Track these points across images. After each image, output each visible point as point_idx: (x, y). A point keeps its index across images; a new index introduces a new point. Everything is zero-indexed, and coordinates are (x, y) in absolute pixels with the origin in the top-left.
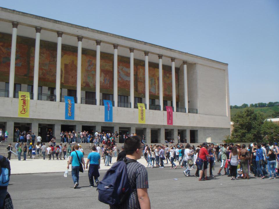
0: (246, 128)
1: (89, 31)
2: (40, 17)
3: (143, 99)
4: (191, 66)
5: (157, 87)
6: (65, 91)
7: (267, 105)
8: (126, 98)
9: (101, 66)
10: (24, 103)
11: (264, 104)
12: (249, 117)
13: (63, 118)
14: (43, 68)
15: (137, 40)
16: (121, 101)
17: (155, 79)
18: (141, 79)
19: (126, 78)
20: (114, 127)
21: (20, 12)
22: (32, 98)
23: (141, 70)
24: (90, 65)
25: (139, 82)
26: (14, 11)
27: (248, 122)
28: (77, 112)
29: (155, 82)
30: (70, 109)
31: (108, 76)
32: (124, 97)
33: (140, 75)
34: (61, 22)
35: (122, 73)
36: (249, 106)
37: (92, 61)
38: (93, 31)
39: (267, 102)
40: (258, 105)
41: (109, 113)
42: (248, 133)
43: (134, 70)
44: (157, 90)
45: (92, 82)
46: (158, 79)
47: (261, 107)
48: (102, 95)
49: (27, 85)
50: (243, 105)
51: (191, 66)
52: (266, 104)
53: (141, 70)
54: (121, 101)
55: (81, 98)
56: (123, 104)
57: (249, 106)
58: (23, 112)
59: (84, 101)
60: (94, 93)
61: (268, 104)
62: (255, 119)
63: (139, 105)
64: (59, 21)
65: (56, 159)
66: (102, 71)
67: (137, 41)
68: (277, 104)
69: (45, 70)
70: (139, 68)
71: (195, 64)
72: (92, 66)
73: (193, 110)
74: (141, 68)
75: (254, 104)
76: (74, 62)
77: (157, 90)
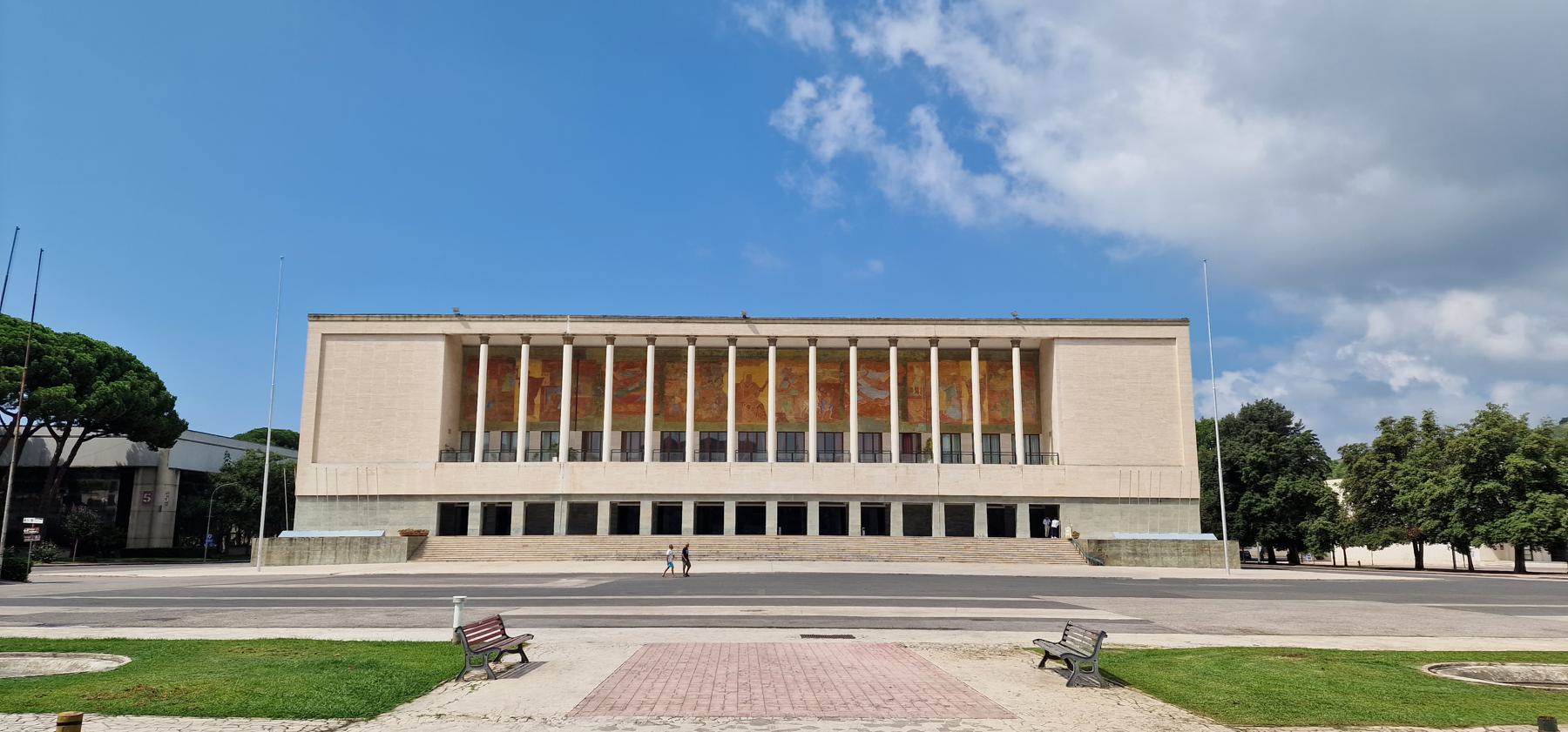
5: (965, 404)
9: (818, 377)
17: (960, 386)
18: (917, 392)
19: (879, 395)
20: (653, 533)
23: (916, 371)
24: (786, 379)
25: (913, 397)
29: (960, 393)
31: (828, 394)
33: (916, 383)
35: (864, 384)
37: (791, 369)
43: (899, 374)
44: (965, 411)
45: (791, 413)
46: (969, 386)
53: (918, 372)
55: (983, 452)
56: (870, 456)
59: (658, 455)
65: (741, 646)
66: (819, 386)
70: (912, 368)
72: (791, 381)
73: (1037, 455)
74: (917, 367)
76: (751, 378)
77: (965, 411)
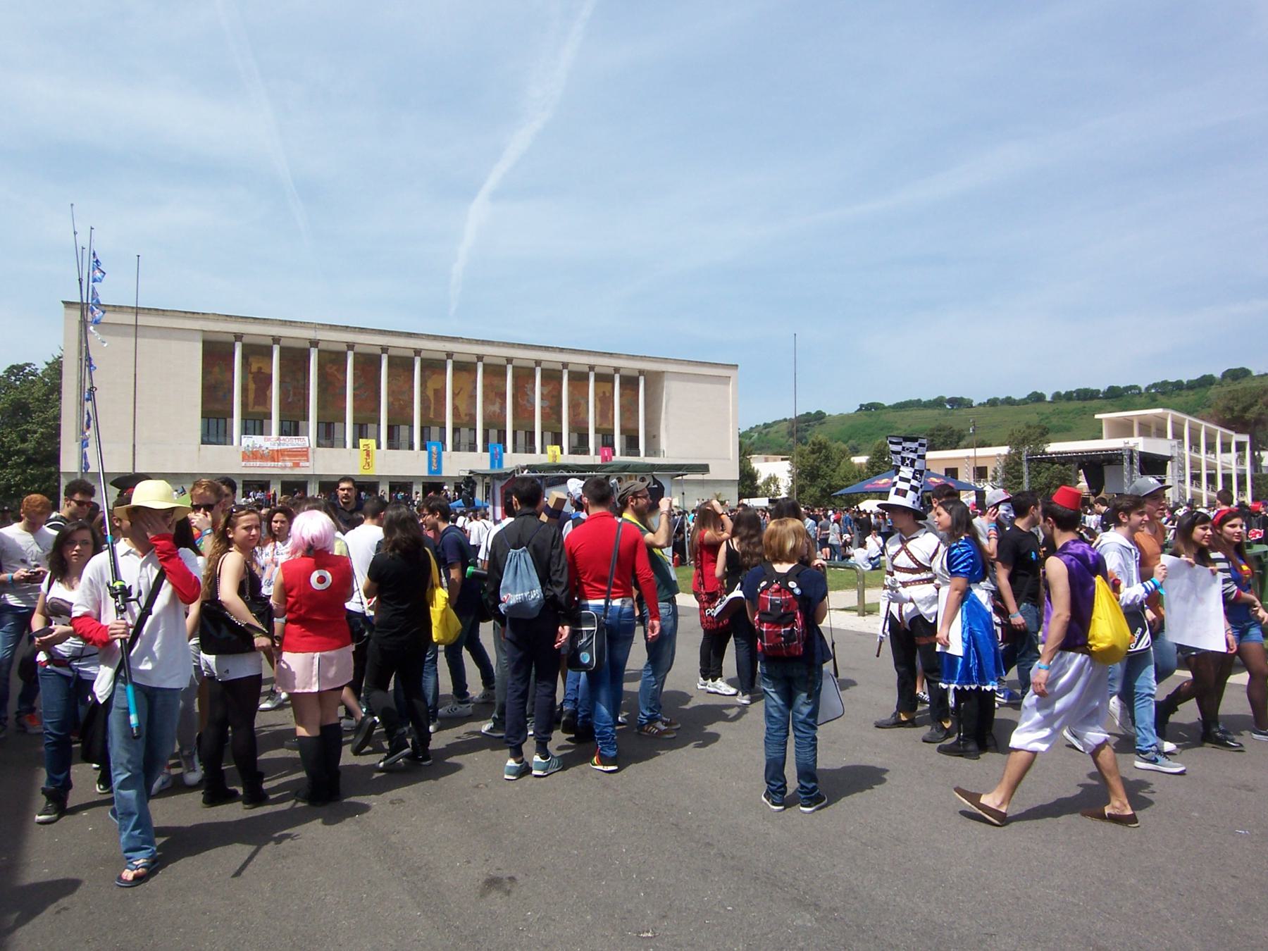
0: (807, 476)
1: (463, 342)
2: (385, 331)
3: (302, 423)
4: (654, 379)
6: (548, 435)
7: (1101, 395)
8: (222, 422)
10: (368, 455)
11: (1093, 391)
12: (815, 456)
13: (426, 474)
14: (400, 397)
15: (545, 347)
16: (208, 432)
21: (356, 328)
22: (378, 447)
26: (347, 327)
27: (811, 466)
28: (445, 463)
30: (435, 461)
32: (215, 420)
34: (417, 334)
36: (1048, 398)
38: (470, 341)
39: (1002, 396)
40: (1075, 395)
41: (497, 459)
42: (811, 485)
47: (1085, 399)
48: (625, 441)
49: (438, 428)
50: (1030, 397)
51: (654, 379)
52: (1099, 391)
54: (208, 432)
57: (1048, 398)
58: (367, 467)
60: (637, 438)
61: (1104, 393)
62: (827, 458)
63: (362, 442)
64: (414, 334)
67: (547, 348)
68: (1133, 391)
69: (403, 400)
71: (663, 372)
75: (1063, 393)
